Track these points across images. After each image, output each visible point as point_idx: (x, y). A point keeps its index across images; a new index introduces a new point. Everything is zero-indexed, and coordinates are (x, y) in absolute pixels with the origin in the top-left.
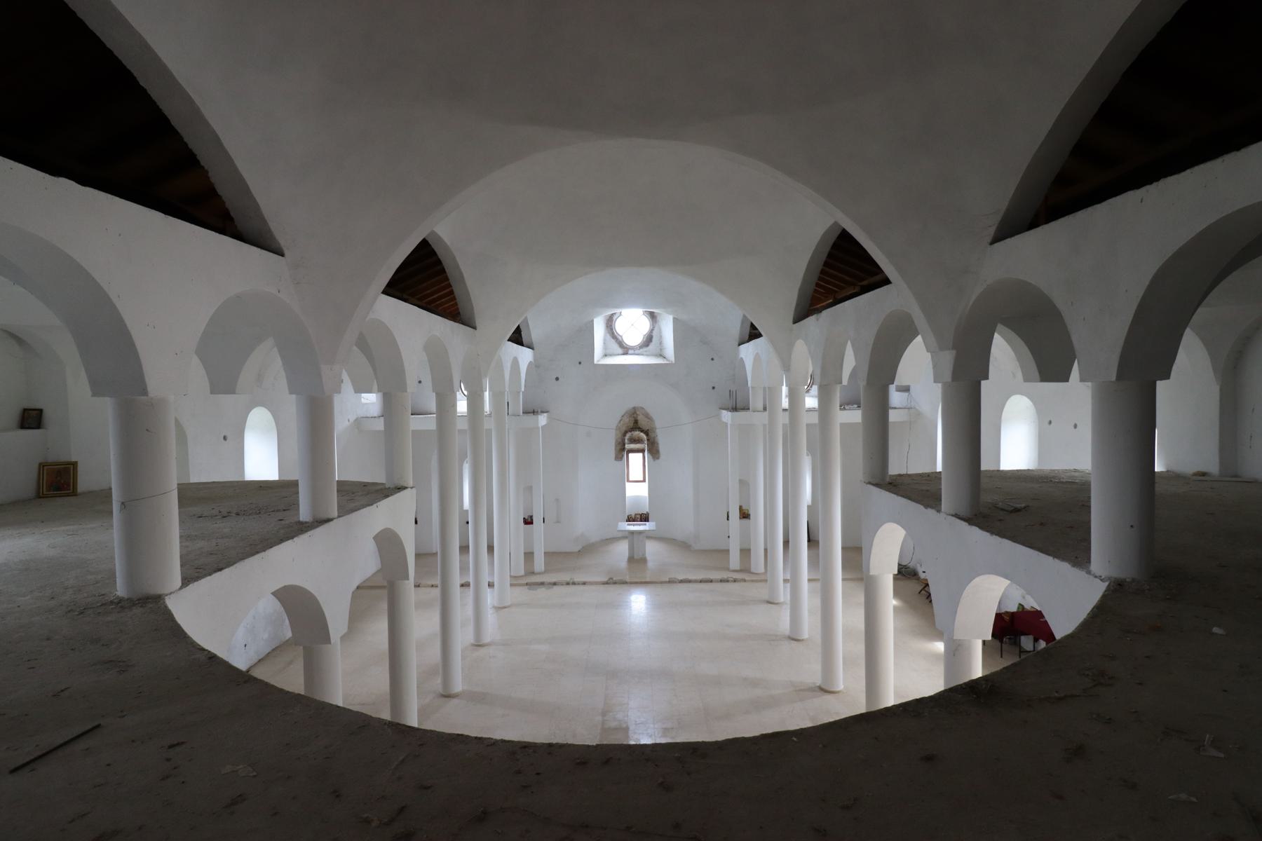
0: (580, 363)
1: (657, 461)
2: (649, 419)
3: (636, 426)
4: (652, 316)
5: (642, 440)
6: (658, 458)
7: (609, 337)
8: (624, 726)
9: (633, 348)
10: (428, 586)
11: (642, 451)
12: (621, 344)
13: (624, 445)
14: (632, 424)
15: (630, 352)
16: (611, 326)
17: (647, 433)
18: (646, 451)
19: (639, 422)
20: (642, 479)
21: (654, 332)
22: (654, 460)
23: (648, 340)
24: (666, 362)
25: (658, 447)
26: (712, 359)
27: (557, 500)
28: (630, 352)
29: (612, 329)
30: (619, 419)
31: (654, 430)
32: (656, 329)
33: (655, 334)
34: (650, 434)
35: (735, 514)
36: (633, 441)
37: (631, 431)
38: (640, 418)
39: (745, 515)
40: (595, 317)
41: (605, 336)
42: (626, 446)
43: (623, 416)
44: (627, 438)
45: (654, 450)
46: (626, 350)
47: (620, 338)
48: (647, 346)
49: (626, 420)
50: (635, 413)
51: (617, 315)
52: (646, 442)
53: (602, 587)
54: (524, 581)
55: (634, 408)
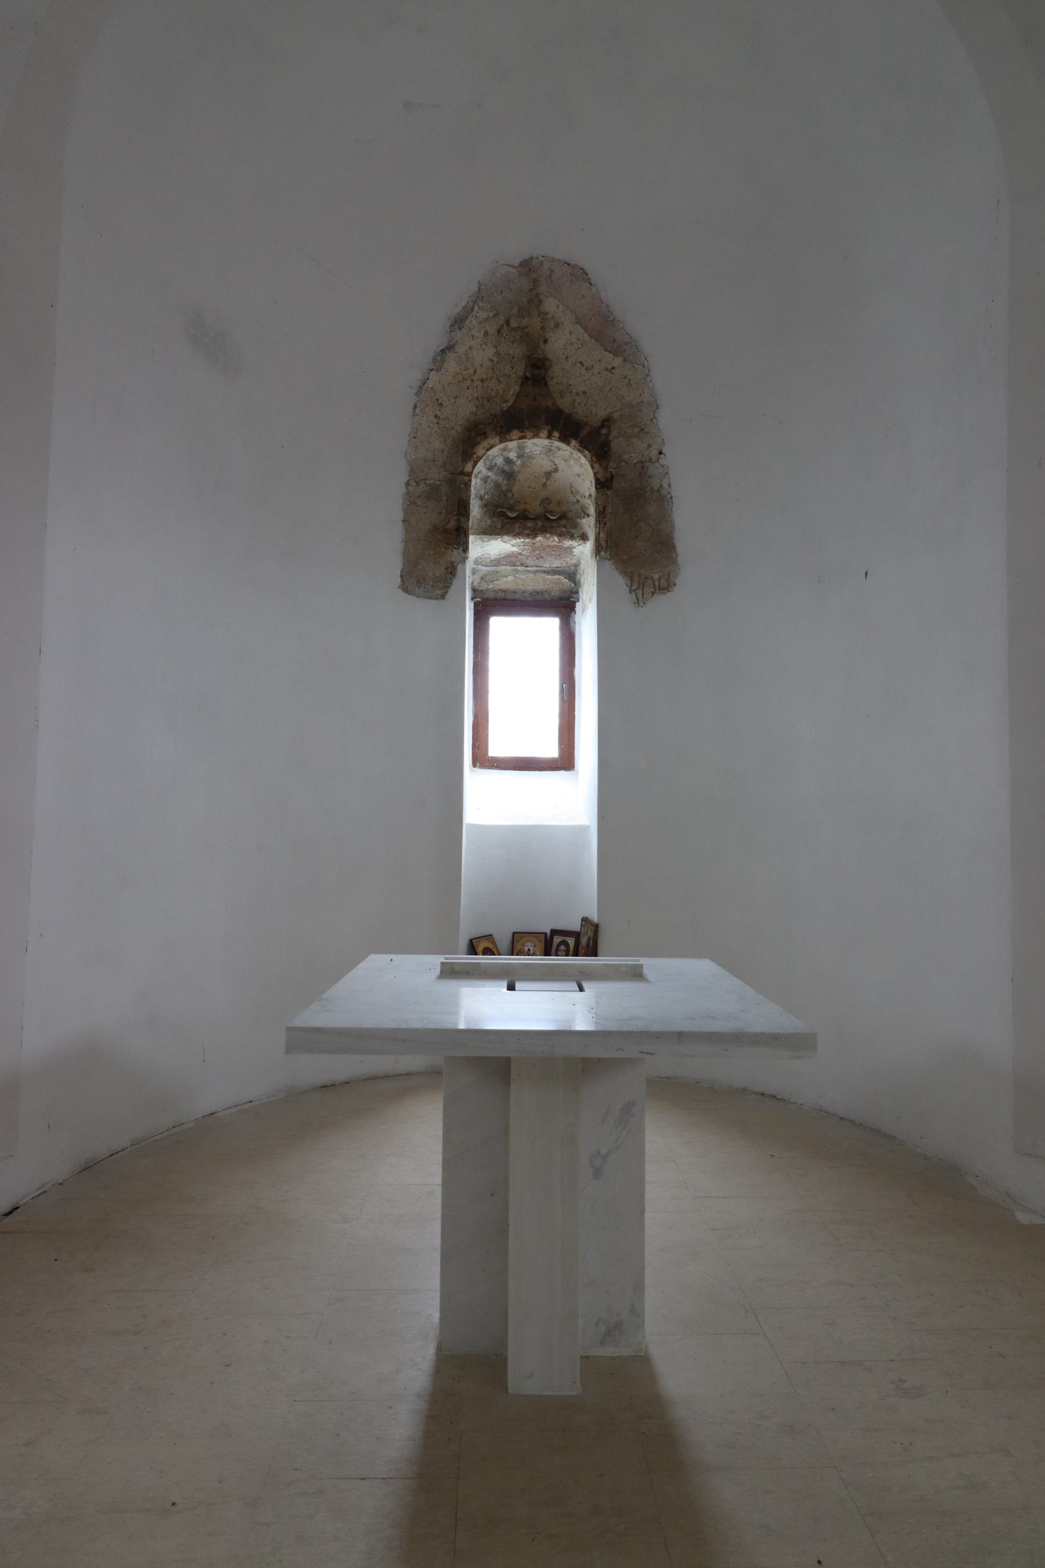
1: (659, 606)
5: (563, 516)
6: (665, 586)
8: (670, 589)
19: (558, 375)
20: (551, 750)
30: (437, 339)
34: (617, 444)
37: (504, 435)
43: (458, 322)
50: (533, 301)
52: (589, 524)
55: (528, 267)
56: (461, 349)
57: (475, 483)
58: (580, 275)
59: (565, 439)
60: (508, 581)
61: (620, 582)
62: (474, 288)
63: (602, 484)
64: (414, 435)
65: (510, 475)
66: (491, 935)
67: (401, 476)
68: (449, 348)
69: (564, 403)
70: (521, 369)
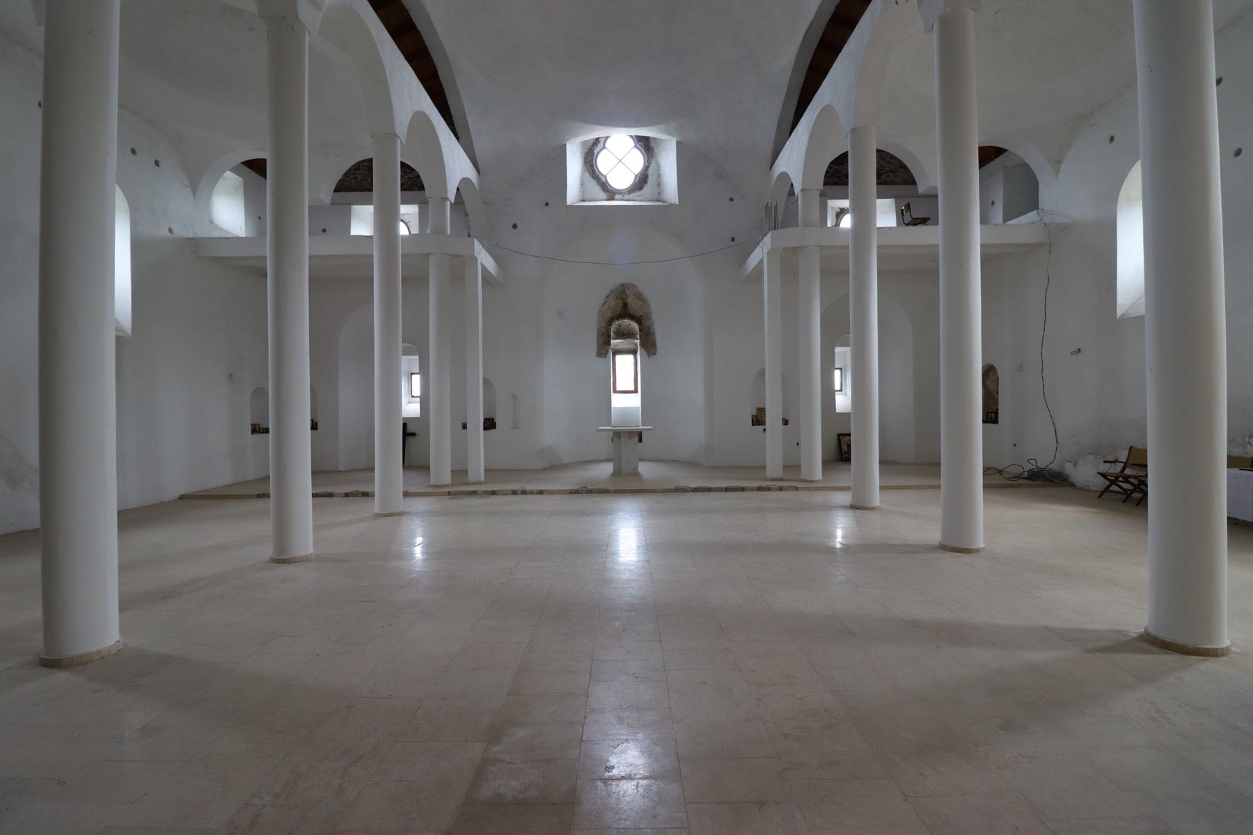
0: (547, 204)
1: (653, 358)
3: (624, 312)
4: (646, 145)
5: (633, 334)
6: (655, 354)
7: (587, 176)
11: (634, 352)
12: (604, 186)
13: (609, 337)
14: (620, 309)
16: (591, 161)
17: (639, 321)
18: (638, 352)
19: (630, 306)
20: (632, 388)
21: (650, 169)
22: (649, 357)
23: (642, 181)
25: (655, 338)
26: (731, 199)
27: (515, 396)
29: (592, 166)
30: (603, 301)
32: (653, 166)
33: (650, 171)
36: (622, 334)
38: (631, 300)
42: (612, 341)
43: (607, 297)
44: (613, 328)
45: (649, 344)
46: (611, 193)
47: (603, 179)
48: (641, 188)
49: (612, 302)
51: (600, 146)
52: (638, 336)
53: (567, 497)
54: (447, 490)
55: (622, 285)
56: (608, 302)
57: (612, 329)
58: (634, 286)
59: (632, 320)
60: (620, 347)
61: (645, 353)
62: (610, 290)
63: (641, 330)
64: (598, 322)
65: (620, 326)
66: (1131, 447)
67: (596, 331)
68: (605, 302)
69: (631, 312)
70: (621, 305)
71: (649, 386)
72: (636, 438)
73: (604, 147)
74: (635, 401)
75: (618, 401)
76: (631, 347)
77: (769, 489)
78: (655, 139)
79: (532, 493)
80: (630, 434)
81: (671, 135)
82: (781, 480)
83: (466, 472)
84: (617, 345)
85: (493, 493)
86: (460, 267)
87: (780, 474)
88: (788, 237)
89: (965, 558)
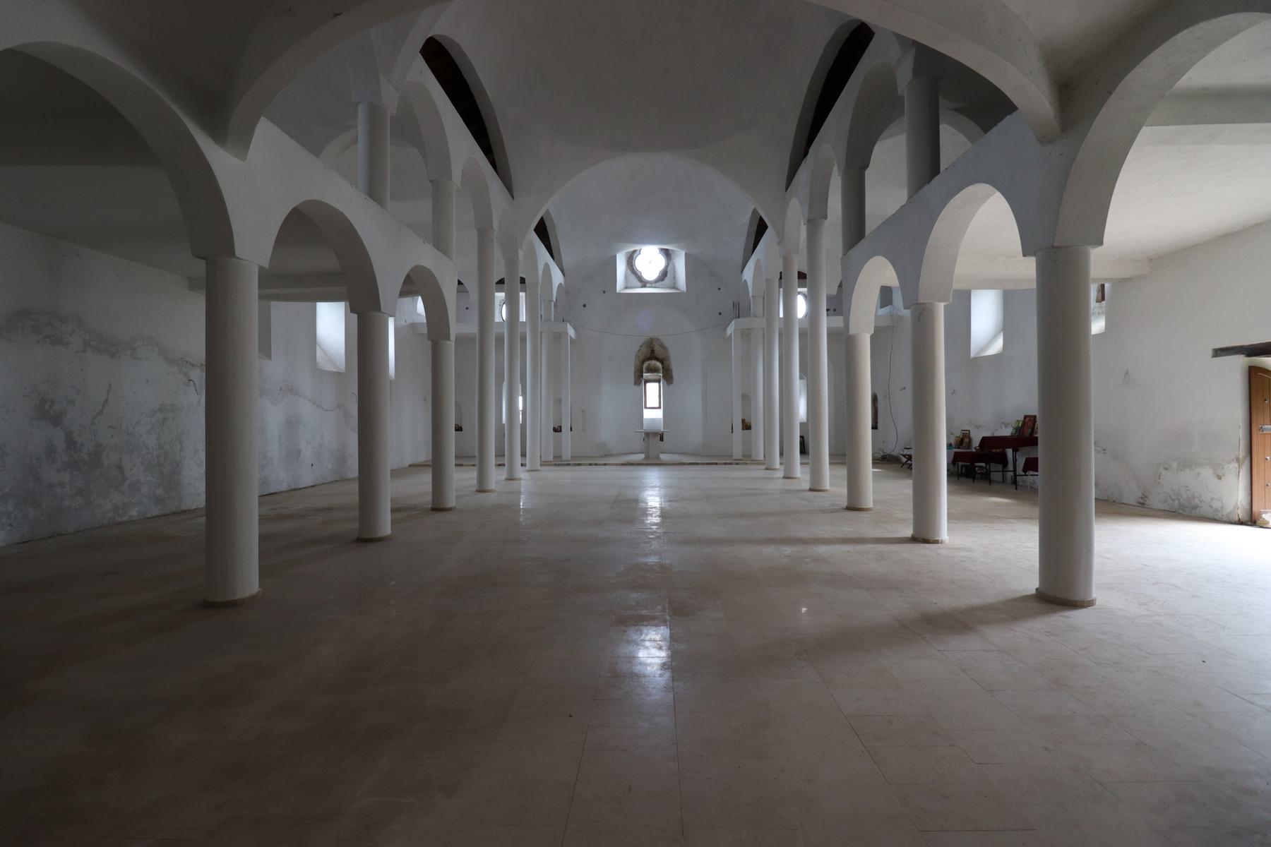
0: (604, 292)
1: (671, 386)
2: (663, 348)
3: (652, 356)
4: (667, 253)
7: (629, 272)
9: (650, 282)
10: (471, 465)
11: (658, 381)
12: (640, 278)
13: (642, 372)
15: (648, 285)
17: (662, 362)
19: (656, 353)
20: (657, 406)
23: (664, 275)
24: (678, 291)
28: (648, 285)
29: (632, 266)
31: (667, 358)
35: (738, 426)
36: (650, 370)
37: (648, 360)
38: (657, 348)
39: (747, 426)
40: (617, 252)
41: (626, 271)
43: (641, 346)
44: (645, 366)
45: (668, 377)
46: (644, 284)
49: (644, 350)
51: (637, 253)
55: (651, 339)
58: (658, 339)
60: (649, 378)
63: (663, 368)
65: (649, 364)
67: (633, 368)
71: (668, 403)
72: (659, 437)
73: (640, 253)
74: (658, 414)
75: (648, 414)
76: (657, 378)
77: (731, 464)
78: (672, 250)
79: (600, 465)
80: (655, 434)
81: (680, 248)
82: (741, 460)
83: (561, 457)
84: (647, 376)
85: (579, 465)
86: (558, 338)
87: (741, 457)
88: (744, 322)
89: (793, 480)
